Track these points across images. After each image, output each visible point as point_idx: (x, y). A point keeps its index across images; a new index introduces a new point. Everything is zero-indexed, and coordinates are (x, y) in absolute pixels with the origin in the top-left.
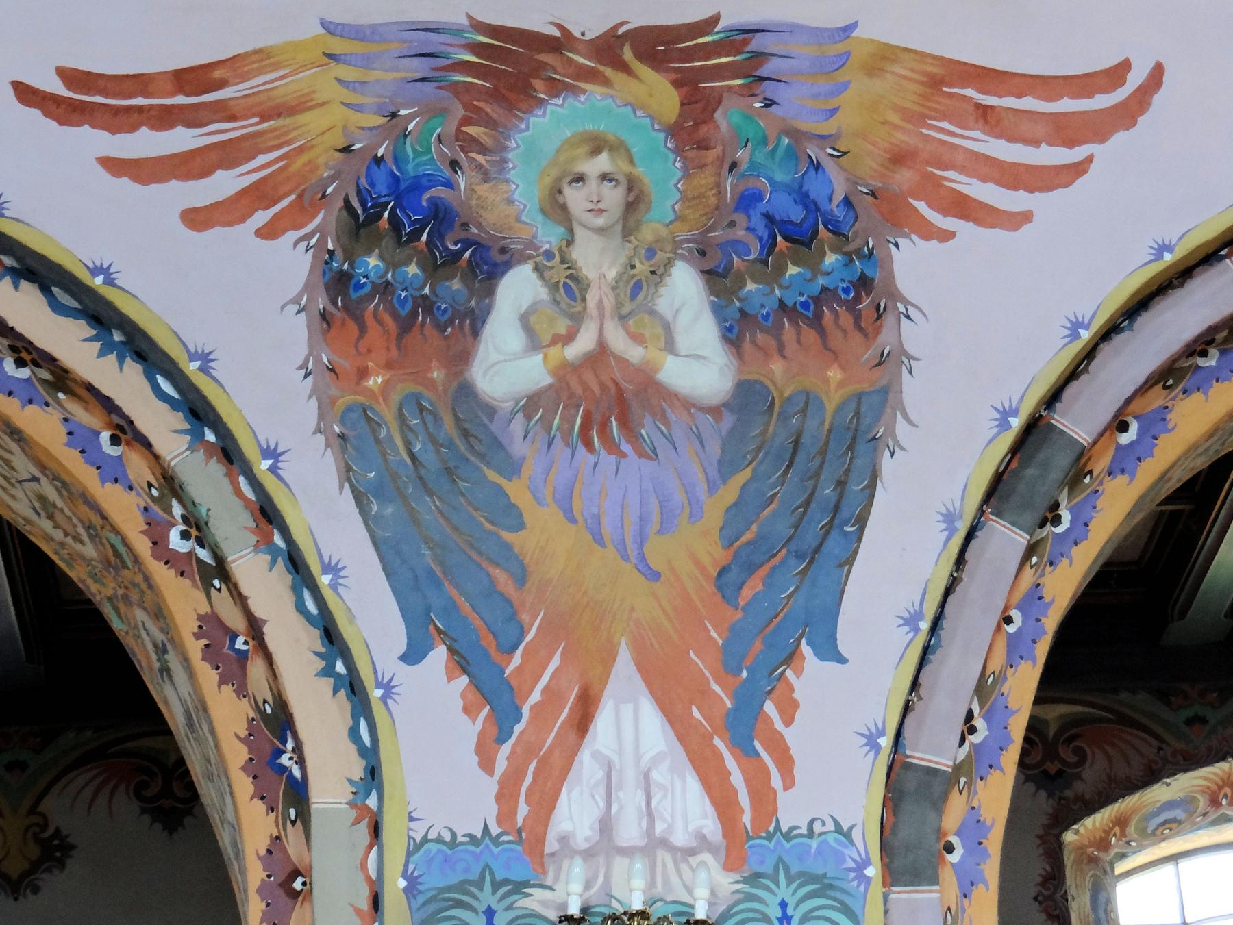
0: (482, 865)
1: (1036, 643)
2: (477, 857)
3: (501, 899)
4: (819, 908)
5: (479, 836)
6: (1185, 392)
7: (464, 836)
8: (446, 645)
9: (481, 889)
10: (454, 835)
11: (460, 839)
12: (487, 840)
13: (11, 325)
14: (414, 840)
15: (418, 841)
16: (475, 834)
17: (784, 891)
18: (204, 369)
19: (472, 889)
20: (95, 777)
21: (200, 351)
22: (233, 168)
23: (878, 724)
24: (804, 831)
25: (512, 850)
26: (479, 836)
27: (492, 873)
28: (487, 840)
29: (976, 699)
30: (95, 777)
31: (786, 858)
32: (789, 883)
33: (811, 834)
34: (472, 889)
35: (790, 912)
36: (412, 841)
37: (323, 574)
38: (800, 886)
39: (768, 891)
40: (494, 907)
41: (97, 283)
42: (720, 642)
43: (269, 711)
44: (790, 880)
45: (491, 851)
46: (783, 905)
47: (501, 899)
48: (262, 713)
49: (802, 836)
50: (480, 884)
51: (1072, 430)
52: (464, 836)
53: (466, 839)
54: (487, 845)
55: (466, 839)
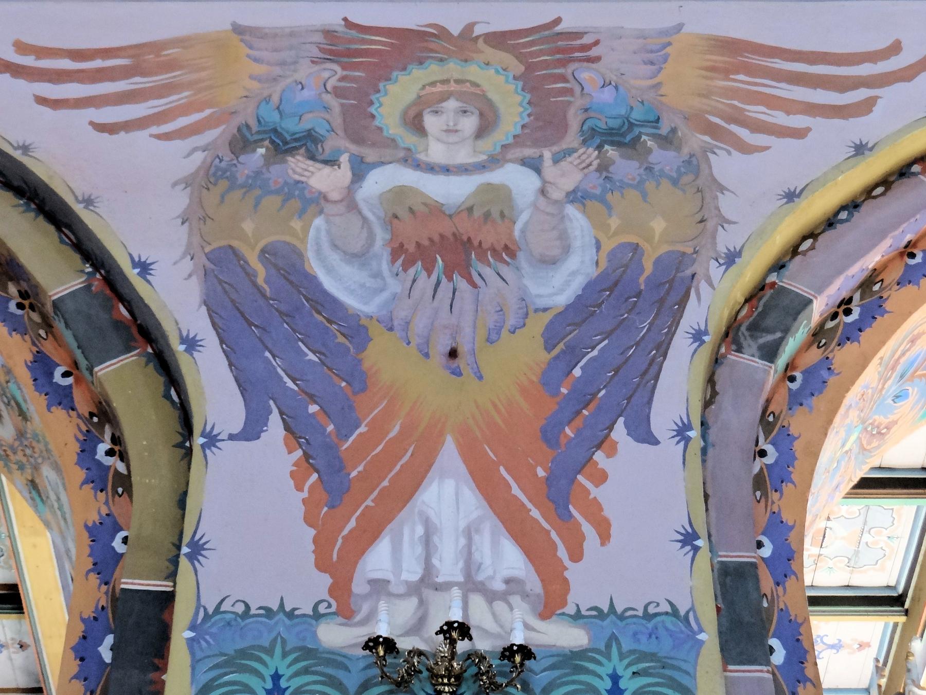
0: (274, 634)
3: (629, 665)
4: (308, 684)
8: (302, 449)
9: (272, 656)
10: (247, 607)
11: (253, 611)
13: (818, 90)
14: (205, 609)
15: (210, 611)
20: (200, 539)
22: (24, 166)
23: (204, 538)
24: (640, 613)
27: (284, 642)
30: (200, 539)
33: (647, 616)
35: (622, 684)
36: (202, 610)
37: (705, 342)
38: (296, 661)
40: (620, 672)
44: (622, 657)
46: (615, 678)
49: (635, 616)
50: (270, 651)
51: (795, 287)
52: (260, 608)
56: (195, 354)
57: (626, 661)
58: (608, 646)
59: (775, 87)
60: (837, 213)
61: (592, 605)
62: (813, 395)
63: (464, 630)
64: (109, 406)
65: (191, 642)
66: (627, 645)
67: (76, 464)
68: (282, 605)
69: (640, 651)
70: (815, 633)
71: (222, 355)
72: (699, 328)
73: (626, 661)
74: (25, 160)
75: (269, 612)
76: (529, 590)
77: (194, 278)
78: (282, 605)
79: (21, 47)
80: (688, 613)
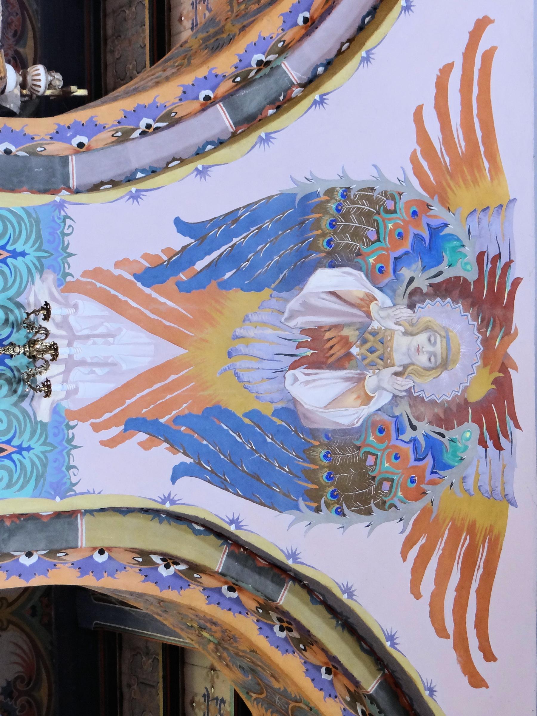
1: (155, 583)
2: (56, 249)
5: (72, 443)
6: (271, 38)
7: (73, 434)
9: (42, 445)
11: (71, 431)
12: (65, 255)
16: (69, 249)
17: (38, 448)
18: (315, 103)
19: (37, 245)
21: (290, 552)
24: (67, 271)
25: (60, 269)
26: (72, 443)
27: (51, 450)
28: (65, 255)
29: (132, 137)
31: (52, 257)
32: (43, 452)
34: (37, 245)
35: (20, 258)
39: (33, 243)
40: (32, 451)
41: (362, 53)
42: (162, 421)
43: (140, 560)
45: (58, 257)
47: (38, 457)
48: (139, 563)
52: (73, 434)
53: (71, 436)
54: (62, 255)
55: (71, 436)
56: (434, 697)
57: (41, 456)
58: (50, 445)
59: (458, 565)
60: (204, 146)
61: (75, 437)
62: (134, 110)
63: (55, 357)
64: (179, 75)
65: (55, 201)
66: (51, 456)
67: (305, 677)
68: (75, 447)
69: (47, 464)
70: (60, 366)
71: (238, 207)
72: (233, 356)
73: (41, 456)
74: (357, 59)
75: (65, 248)
76: (80, 303)
77: (293, 186)
78: (75, 447)
79: (488, 56)
80: (75, 491)
